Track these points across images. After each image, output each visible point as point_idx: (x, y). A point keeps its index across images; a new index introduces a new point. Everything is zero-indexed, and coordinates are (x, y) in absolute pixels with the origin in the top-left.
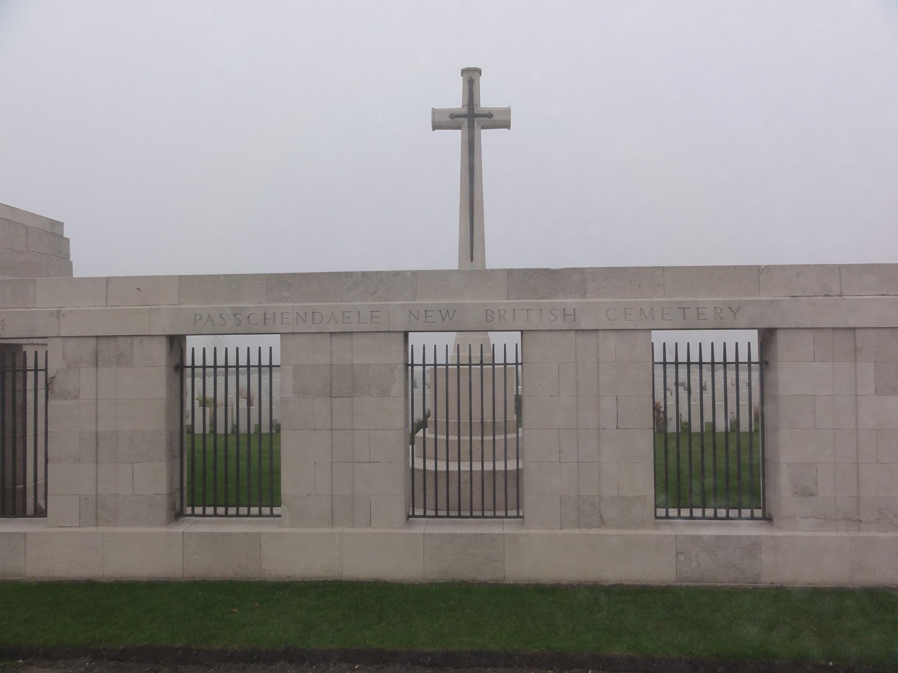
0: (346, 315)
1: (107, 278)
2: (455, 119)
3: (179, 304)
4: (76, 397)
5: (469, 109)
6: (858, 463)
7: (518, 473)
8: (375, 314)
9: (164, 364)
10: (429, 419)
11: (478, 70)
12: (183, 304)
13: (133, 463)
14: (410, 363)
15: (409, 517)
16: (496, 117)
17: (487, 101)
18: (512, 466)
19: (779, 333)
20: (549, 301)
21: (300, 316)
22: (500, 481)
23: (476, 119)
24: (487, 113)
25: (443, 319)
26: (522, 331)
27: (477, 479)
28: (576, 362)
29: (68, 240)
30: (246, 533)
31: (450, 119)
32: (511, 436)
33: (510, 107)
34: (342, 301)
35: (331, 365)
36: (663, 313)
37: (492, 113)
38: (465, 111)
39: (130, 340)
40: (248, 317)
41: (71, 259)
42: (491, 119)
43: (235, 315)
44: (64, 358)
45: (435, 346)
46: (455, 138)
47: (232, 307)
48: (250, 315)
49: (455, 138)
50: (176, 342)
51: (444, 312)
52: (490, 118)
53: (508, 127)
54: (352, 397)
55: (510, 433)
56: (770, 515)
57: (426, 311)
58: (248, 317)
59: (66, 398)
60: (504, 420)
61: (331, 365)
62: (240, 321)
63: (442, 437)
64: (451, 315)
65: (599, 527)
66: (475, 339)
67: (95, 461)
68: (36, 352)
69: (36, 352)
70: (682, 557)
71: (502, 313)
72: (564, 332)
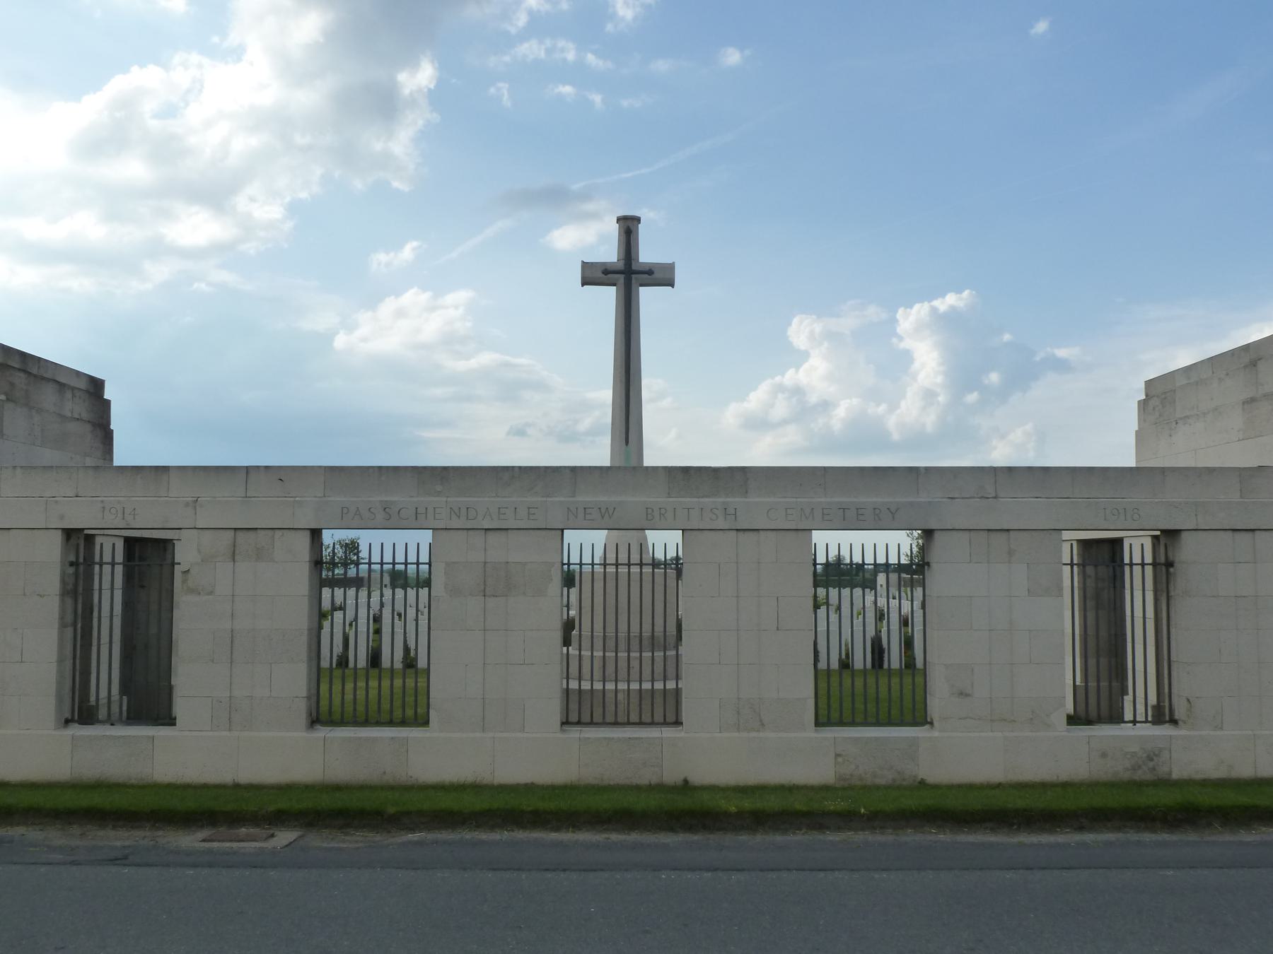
0: (502, 511)
1: (247, 467)
2: (610, 276)
3: (325, 496)
4: (211, 593)
5: (625, 265)
6: (737, 563)
7: (677, 692)
8: (532, 511)
9: (308, 559)
10: (573, 632)
11: (636, 219)
12: (328, 497)
13: (271, 664)
14: (565, 561)
15: (563, 724)
16: (657, 275)
17: (647, 254)
18: (671, 685)
19: (1184, 535)
20: (711, 500)
21: (454, 512)
22: (659, 700)
23: (633, 276)
24: (647, 269)
25: (603, 518)
26: (683, 530)
27: (634, 700)
28: (737, 563)
29: (108, 403)
30: (392, 738)
31: (603, 275)
32: (671, 653)
33: (674, 263)
34: (498, 497)
35: (485, 563)
36: (823, 514)
37: (653, 269)
38: (621, 266)
39: (270, 532)
40: (399, 512)
41: (112, 427)
42: (654, 276)
43: (370, 509)
44: (199, 551)
45: (593, 544)
46: (608, 296)
47: (382, 501)
48: (400, 509)
49: (608, 296)
50: (316, 534)
51: (603, 511)
52: (650, 275)
53: (672, 285)
54: (507, 596)
55: (670, 650)
56: (932, 719)
57: (585, 508)
58: (399, 512)
59: (199, 594)
60: (663, 634)
61: (485, 563)
62: (390, 516)
63: (586, 653)
64: (611, 512)
65: (758, 731)
66: (632, 536)
67: (229, 661)
68: (114, 544)
69: (114, 544)
70: (840, 760)
71: (663, 511)
72: (725, 531)
